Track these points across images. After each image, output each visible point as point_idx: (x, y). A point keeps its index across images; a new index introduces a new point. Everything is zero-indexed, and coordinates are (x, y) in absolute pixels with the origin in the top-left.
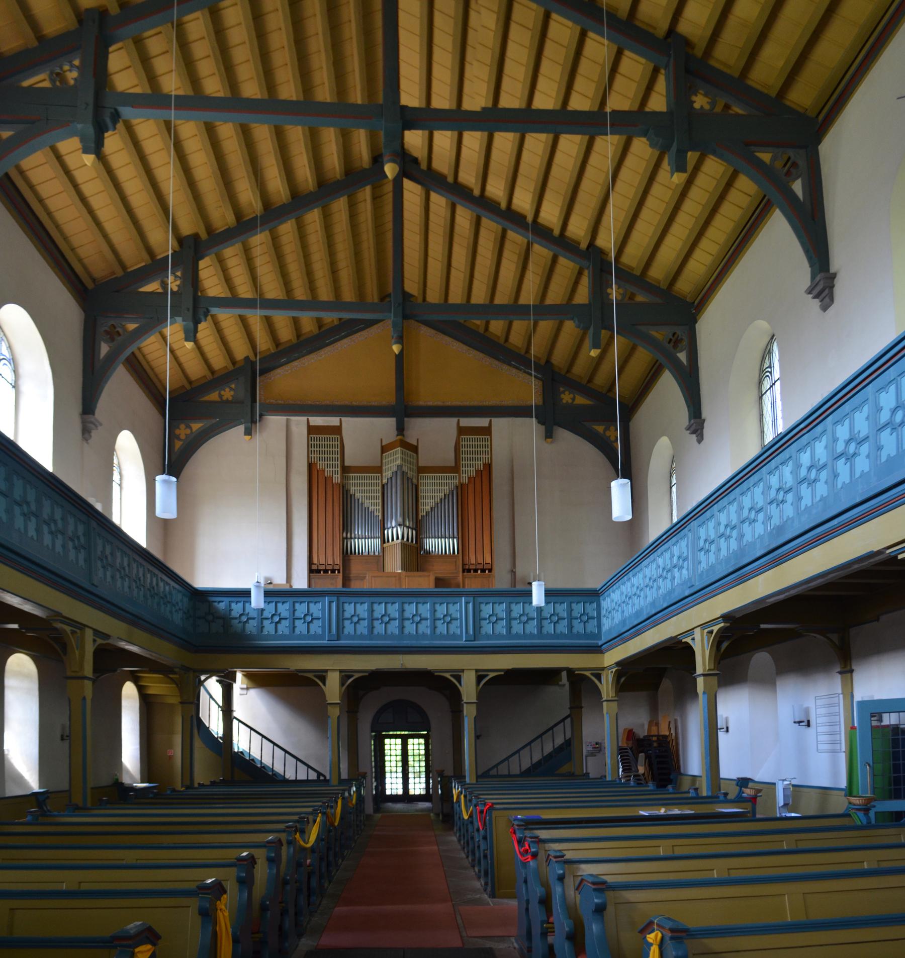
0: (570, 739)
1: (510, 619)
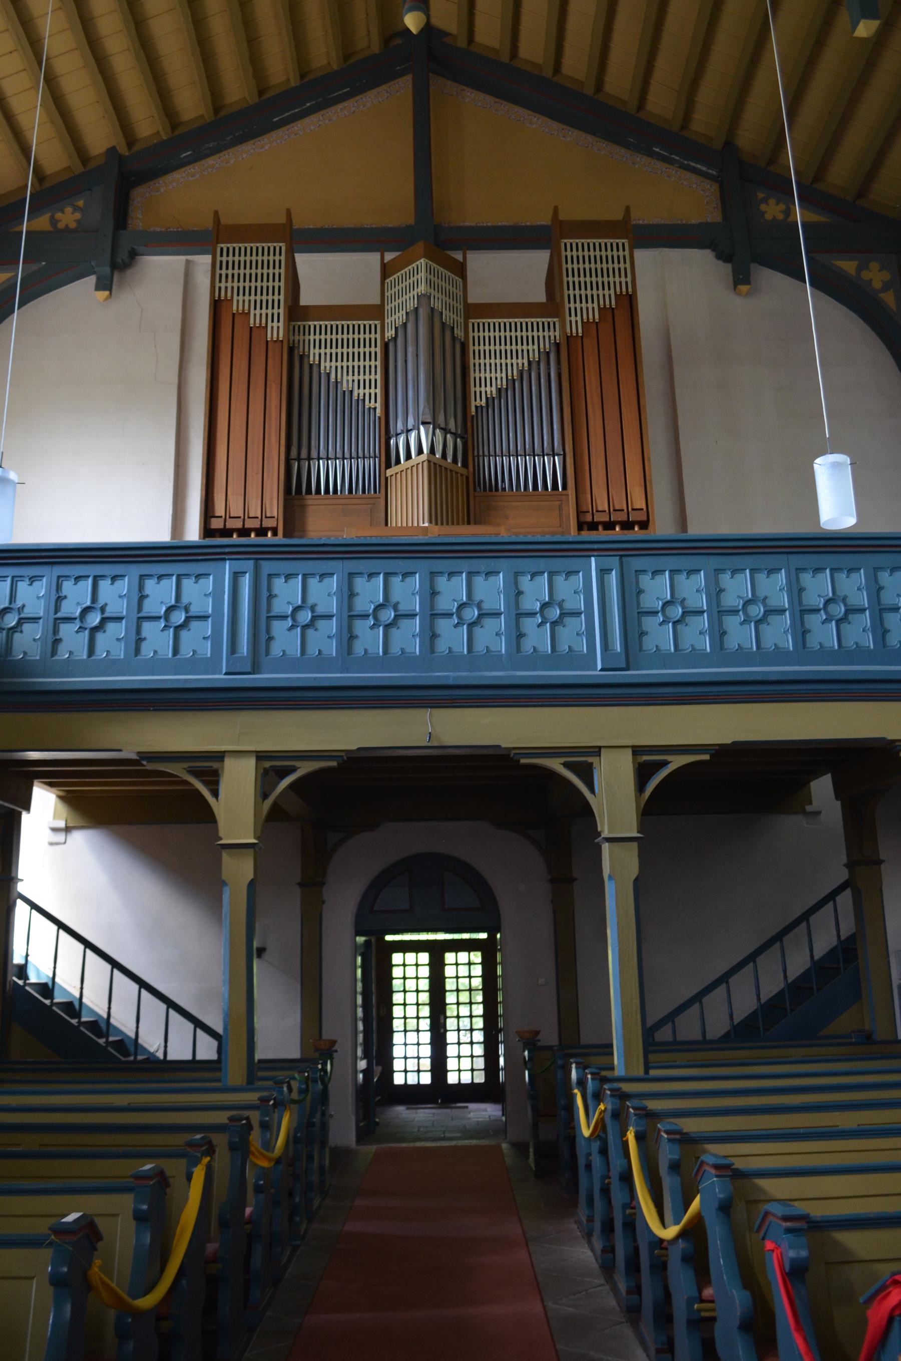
0: (852, 938)
1: (719, 613)
